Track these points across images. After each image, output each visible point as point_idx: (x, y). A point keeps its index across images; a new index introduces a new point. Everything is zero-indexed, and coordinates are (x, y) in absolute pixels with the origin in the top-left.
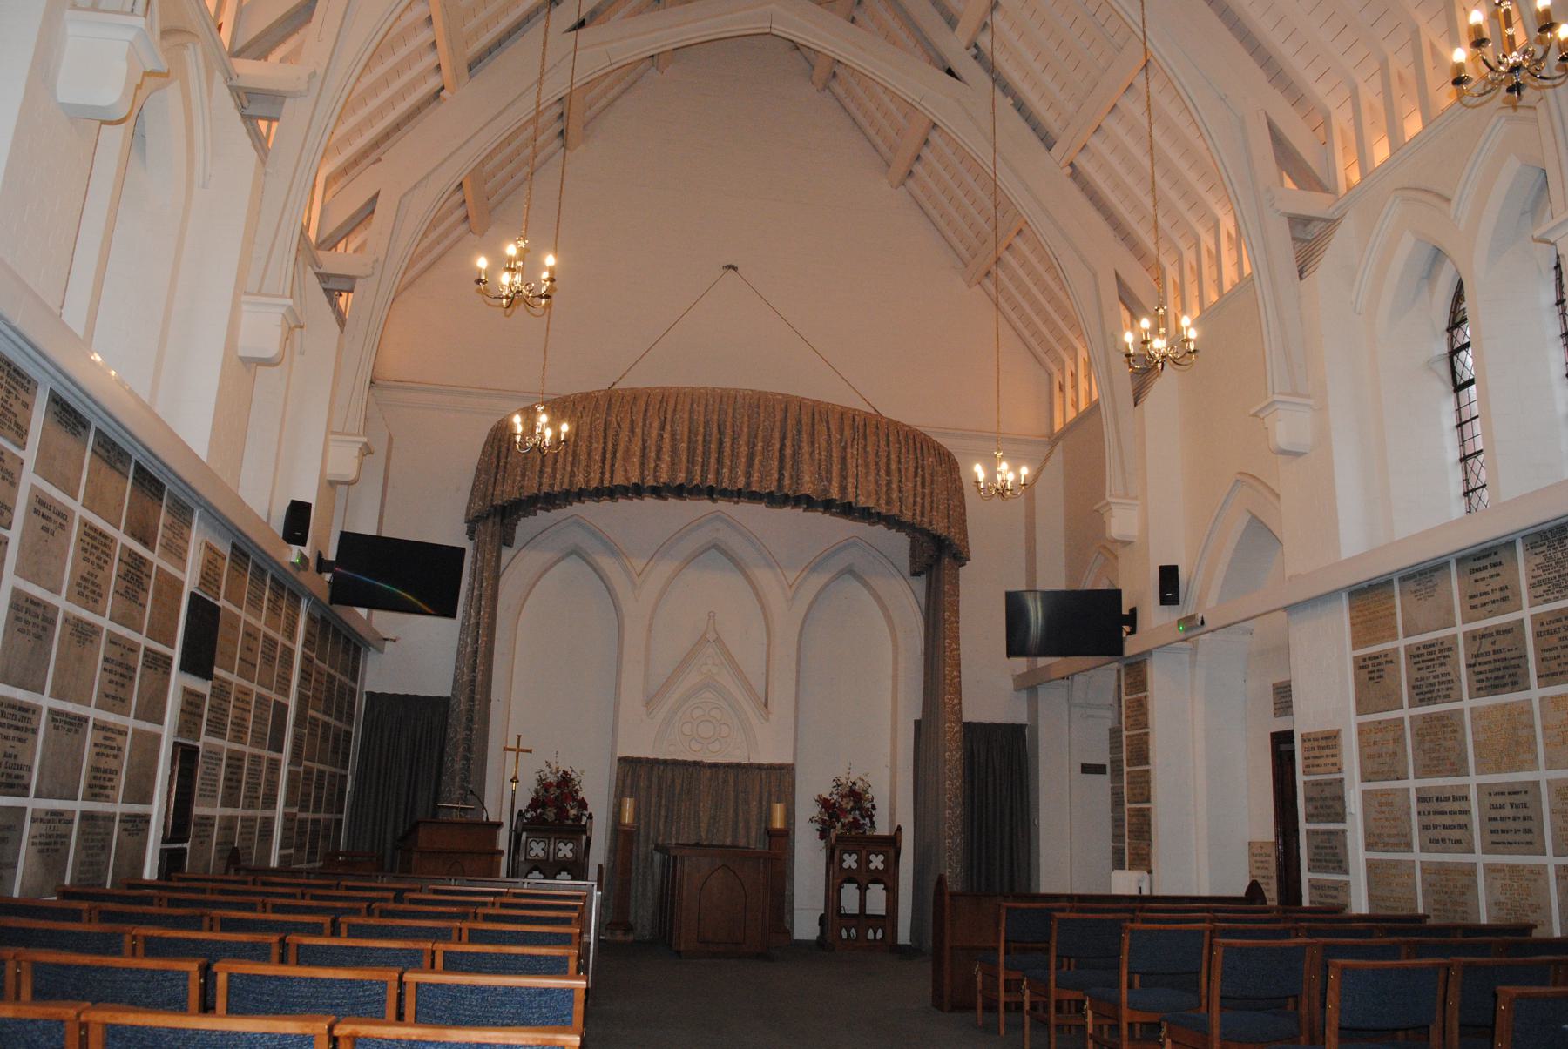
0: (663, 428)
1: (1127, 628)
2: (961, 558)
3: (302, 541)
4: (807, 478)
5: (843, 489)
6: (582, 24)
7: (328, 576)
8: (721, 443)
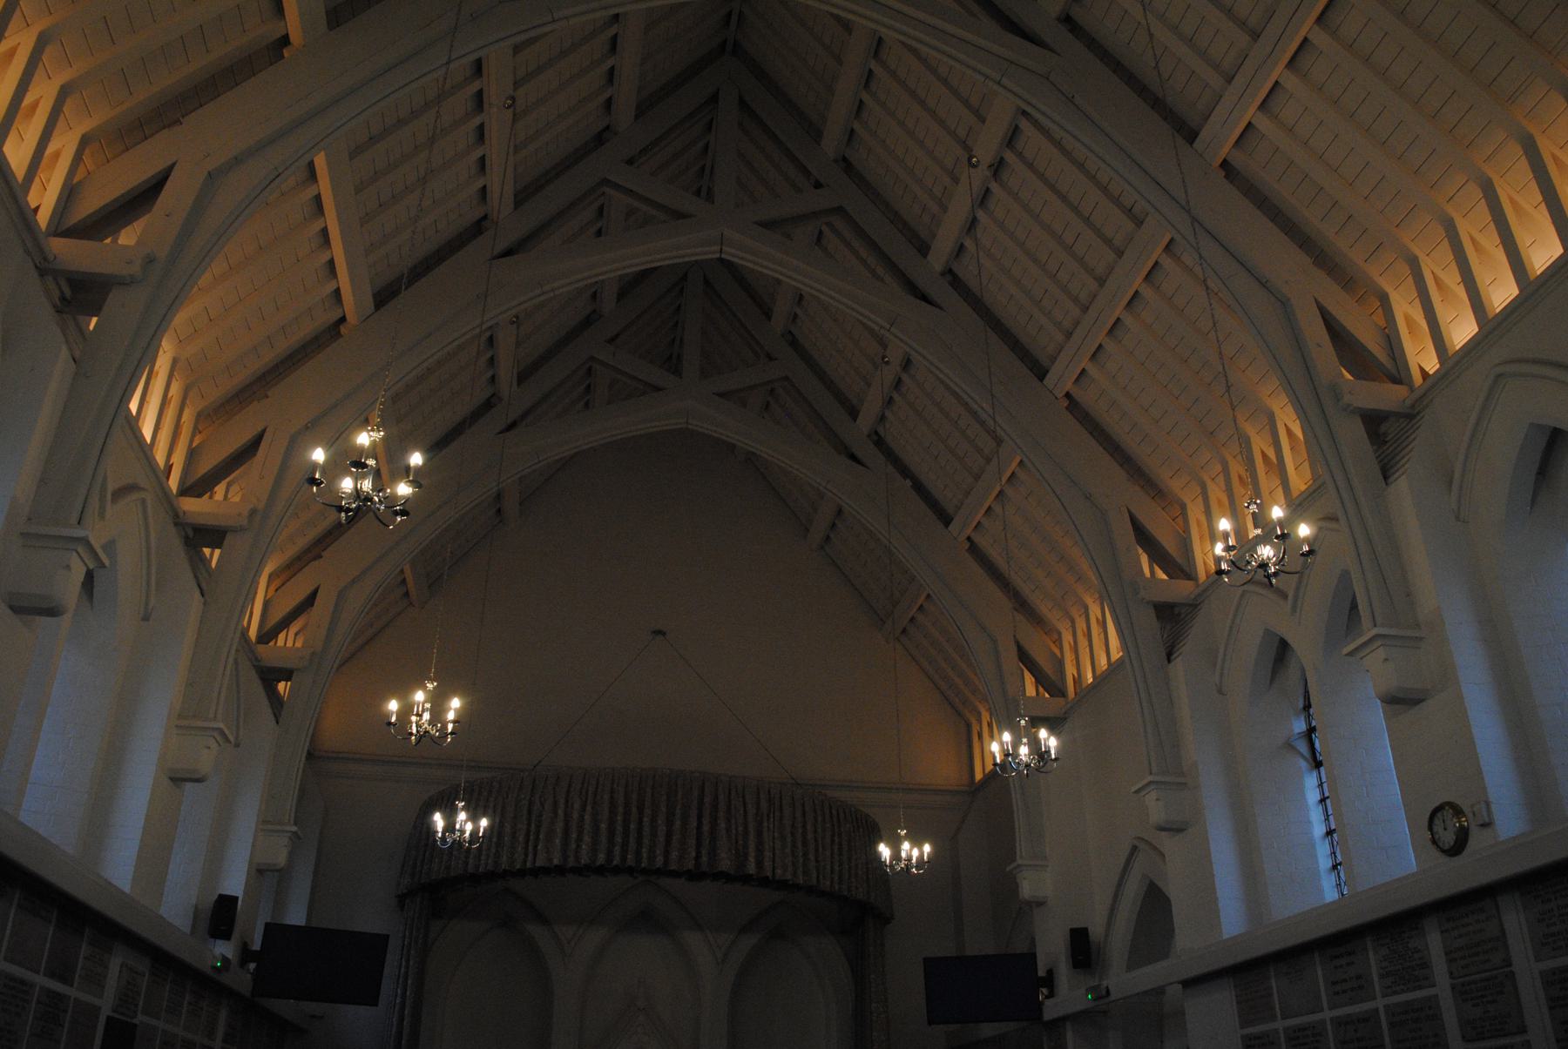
0: (583, 809)
1: (1045, 990)
2: (885, 919)
3: (226, 936)
4: (723, 855)
5: (760, 864)
6: (511, 426)
7: (252, 966)
8: (640, 822)
